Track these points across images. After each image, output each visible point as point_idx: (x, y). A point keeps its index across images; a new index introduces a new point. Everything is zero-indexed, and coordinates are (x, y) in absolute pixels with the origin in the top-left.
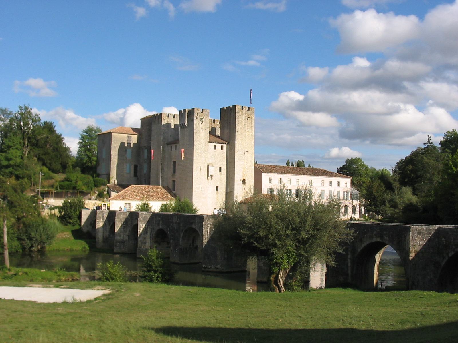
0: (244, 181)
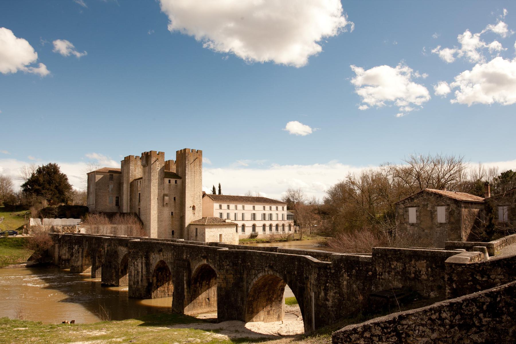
0: (194, 208)
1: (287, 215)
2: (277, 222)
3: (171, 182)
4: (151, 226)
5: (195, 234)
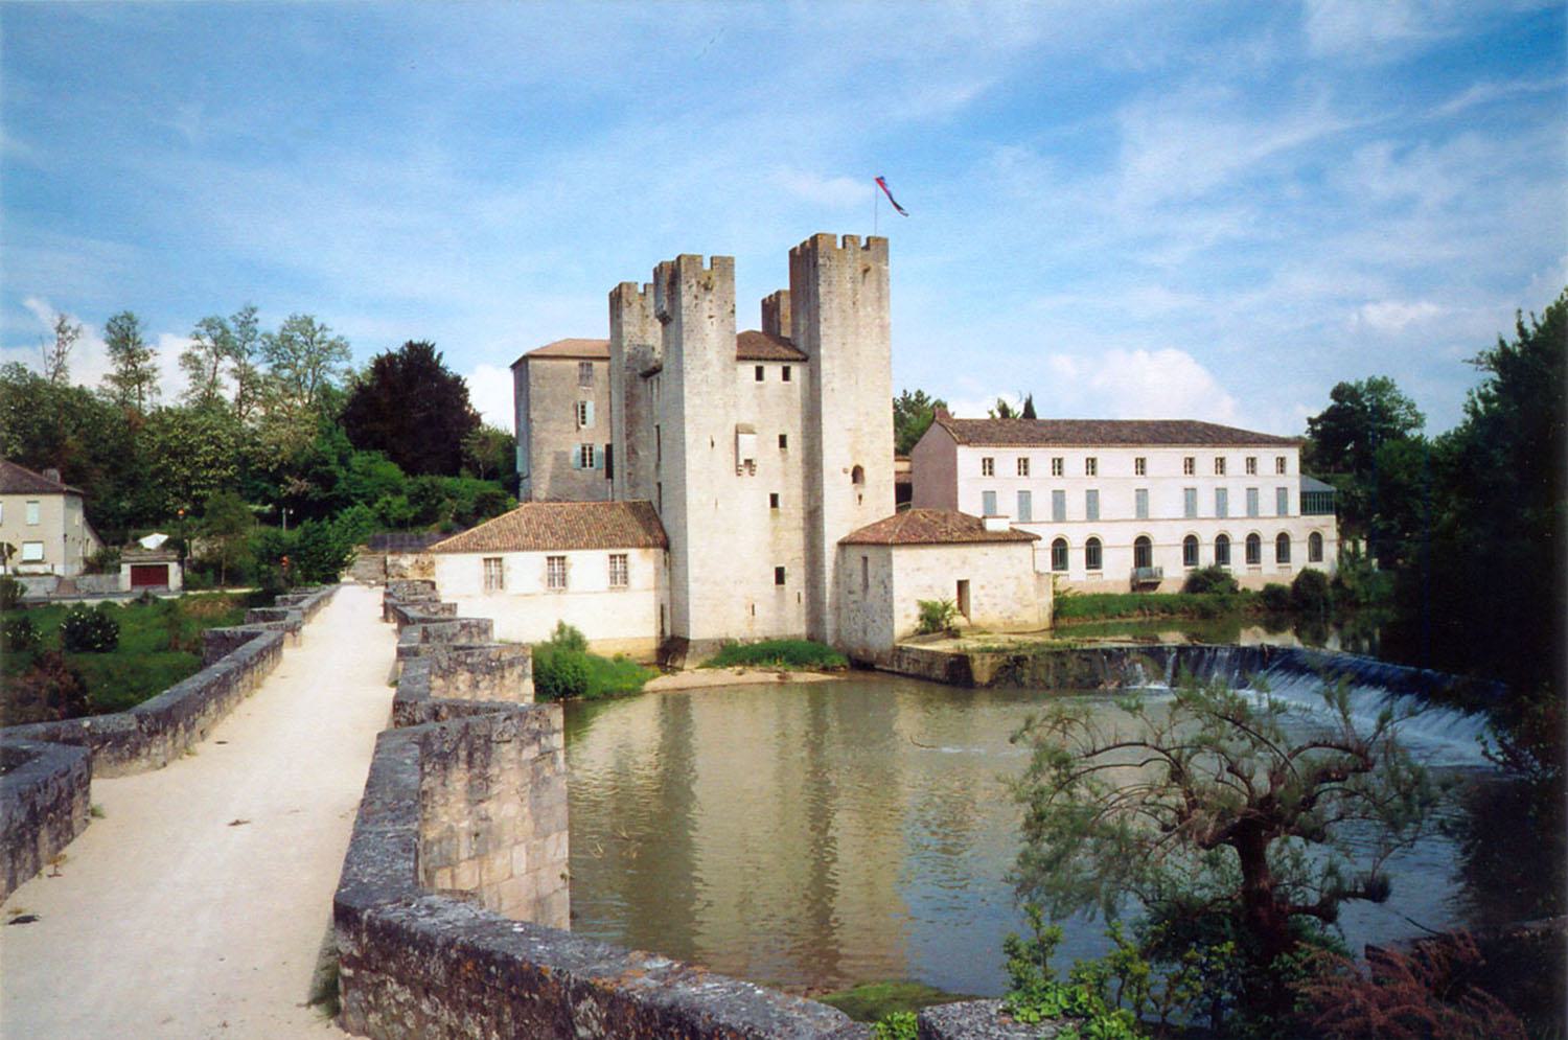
0: (857, 474)
1: (1304, 495)
2: (1251, 526)
3: (1228, 464)
4: (691, 551)
5: (860, 580)
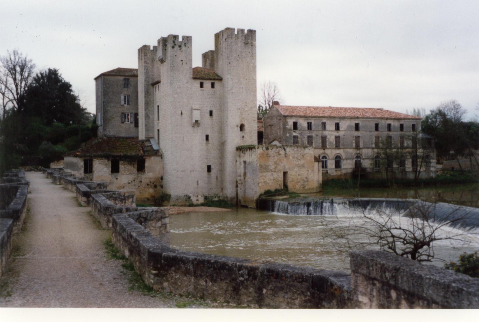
0: (242, 127)
